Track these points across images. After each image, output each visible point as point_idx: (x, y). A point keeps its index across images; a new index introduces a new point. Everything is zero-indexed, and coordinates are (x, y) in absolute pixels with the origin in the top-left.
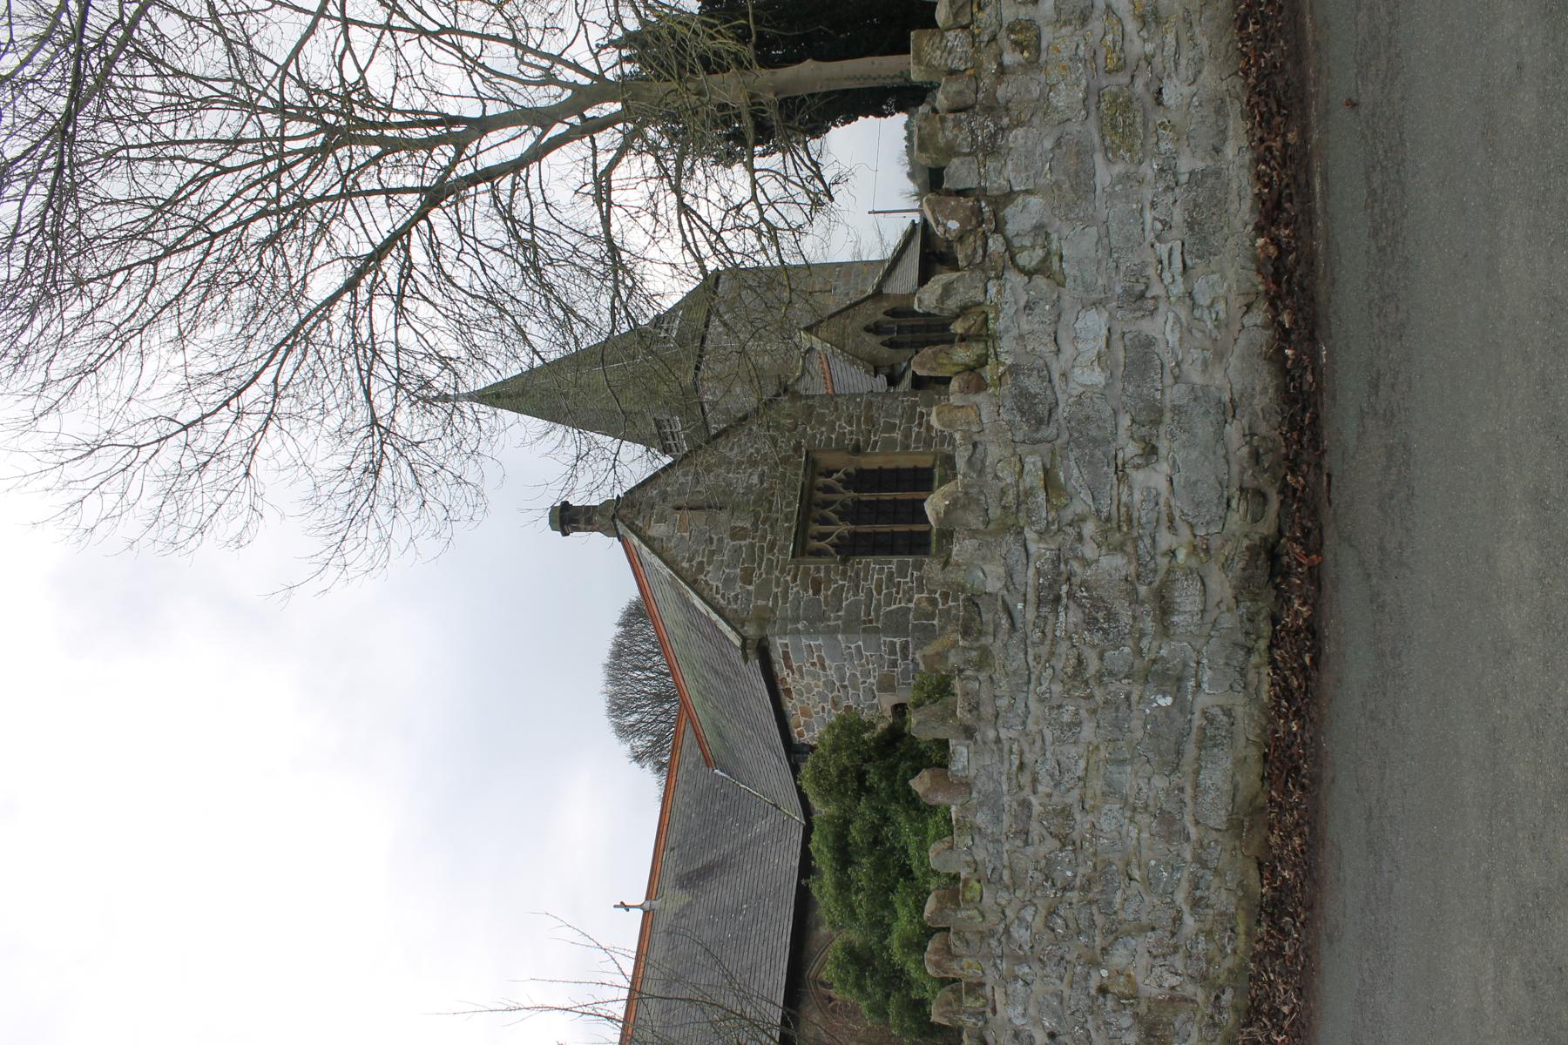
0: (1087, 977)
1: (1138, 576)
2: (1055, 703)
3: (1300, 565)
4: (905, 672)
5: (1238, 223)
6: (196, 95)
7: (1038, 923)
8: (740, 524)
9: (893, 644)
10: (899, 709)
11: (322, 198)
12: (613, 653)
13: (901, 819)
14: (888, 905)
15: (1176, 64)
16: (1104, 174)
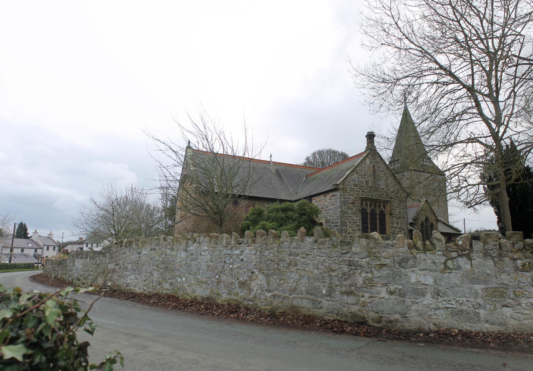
0: (257, 268)
2: (323, 264)
3: (360, 330)
4: (330, 226)
5: (462, 325)
6: (510, 6)
8: (370, 183)
10: (321, 224)
11: (471, 54)
13: (294, 224)
14: (273, 221)
15: (518, 313)
16: (478, 288)
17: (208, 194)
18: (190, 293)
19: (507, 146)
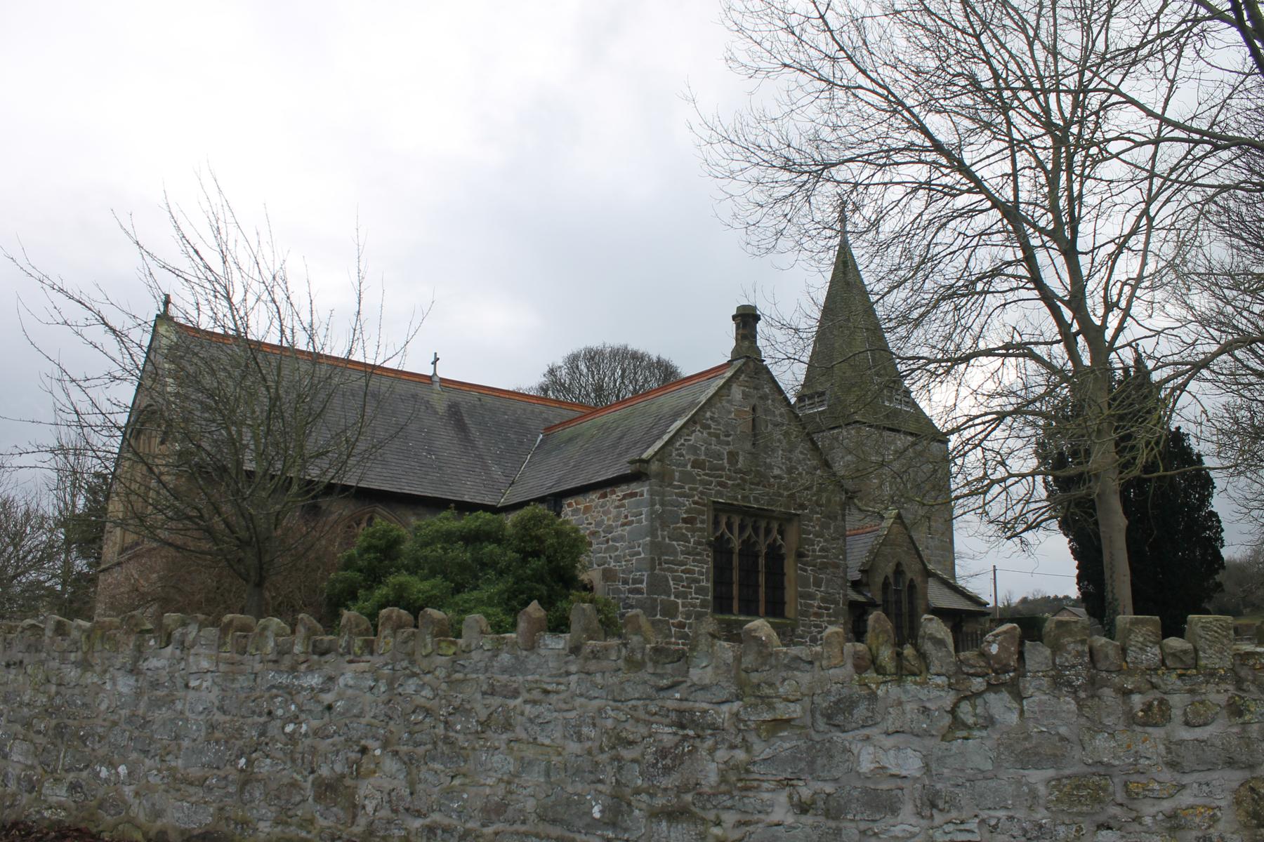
0: (375, 738)
1: (700, 794)
2: (597, 721)
7: (420, 700)
8: (741, 459)
9: (641, 582)
11: (1009, 123)
12: (636, 353)
13: (501, 586)
14: (433, 573)
16: (1037, 777)
17: (222, 478)
18: (142, 818)
19: (1126, 370)
